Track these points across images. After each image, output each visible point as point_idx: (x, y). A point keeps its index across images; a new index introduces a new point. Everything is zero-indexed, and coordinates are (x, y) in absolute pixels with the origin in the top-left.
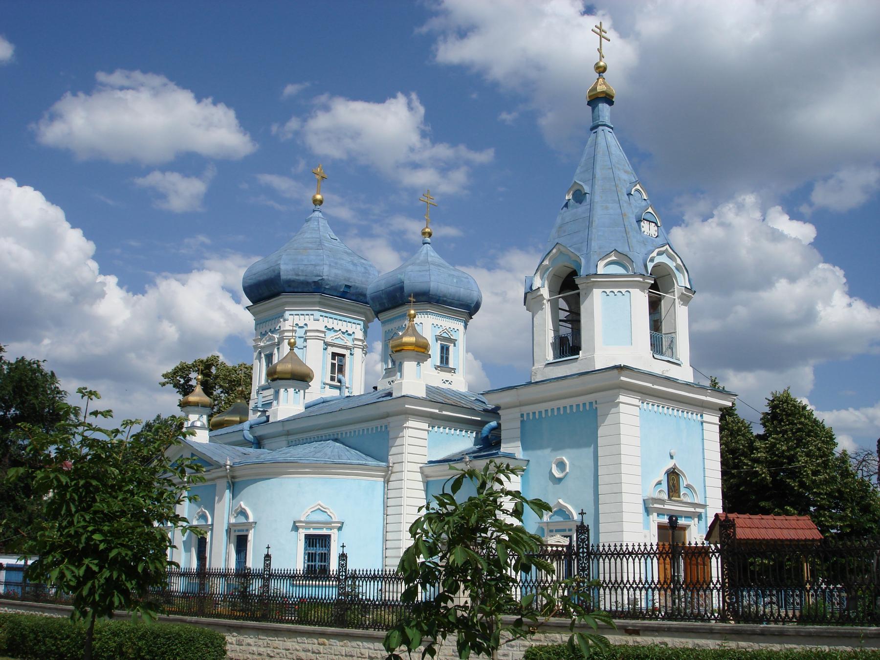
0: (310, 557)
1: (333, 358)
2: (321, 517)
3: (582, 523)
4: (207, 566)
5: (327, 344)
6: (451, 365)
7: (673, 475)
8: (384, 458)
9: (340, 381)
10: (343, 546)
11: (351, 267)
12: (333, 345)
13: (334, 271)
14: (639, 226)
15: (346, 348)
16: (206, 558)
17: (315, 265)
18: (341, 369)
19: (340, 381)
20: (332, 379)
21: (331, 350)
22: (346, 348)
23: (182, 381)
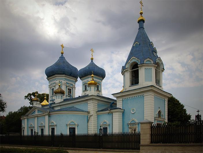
0: (70, 132)
1: (68, 90)
2: (73, 124)
3: (198, 114)
4: (22, 134)
5: (67, 87)
6: (99, 90)
7: (160, 112)
8: (132, 85)
9: (70, 95)
10: (198, 111)
11: (72, 68)
12: (68, 87)
13: (68, 69)
14: (153, 52)
15: (71, 87)
16: (29, 145)
17: (64, 67)
18: (70, 92)
19: (70, 95)
20: (68, 94)
21: (68, 88)
22: (71, 87)
23: (29, 98)
